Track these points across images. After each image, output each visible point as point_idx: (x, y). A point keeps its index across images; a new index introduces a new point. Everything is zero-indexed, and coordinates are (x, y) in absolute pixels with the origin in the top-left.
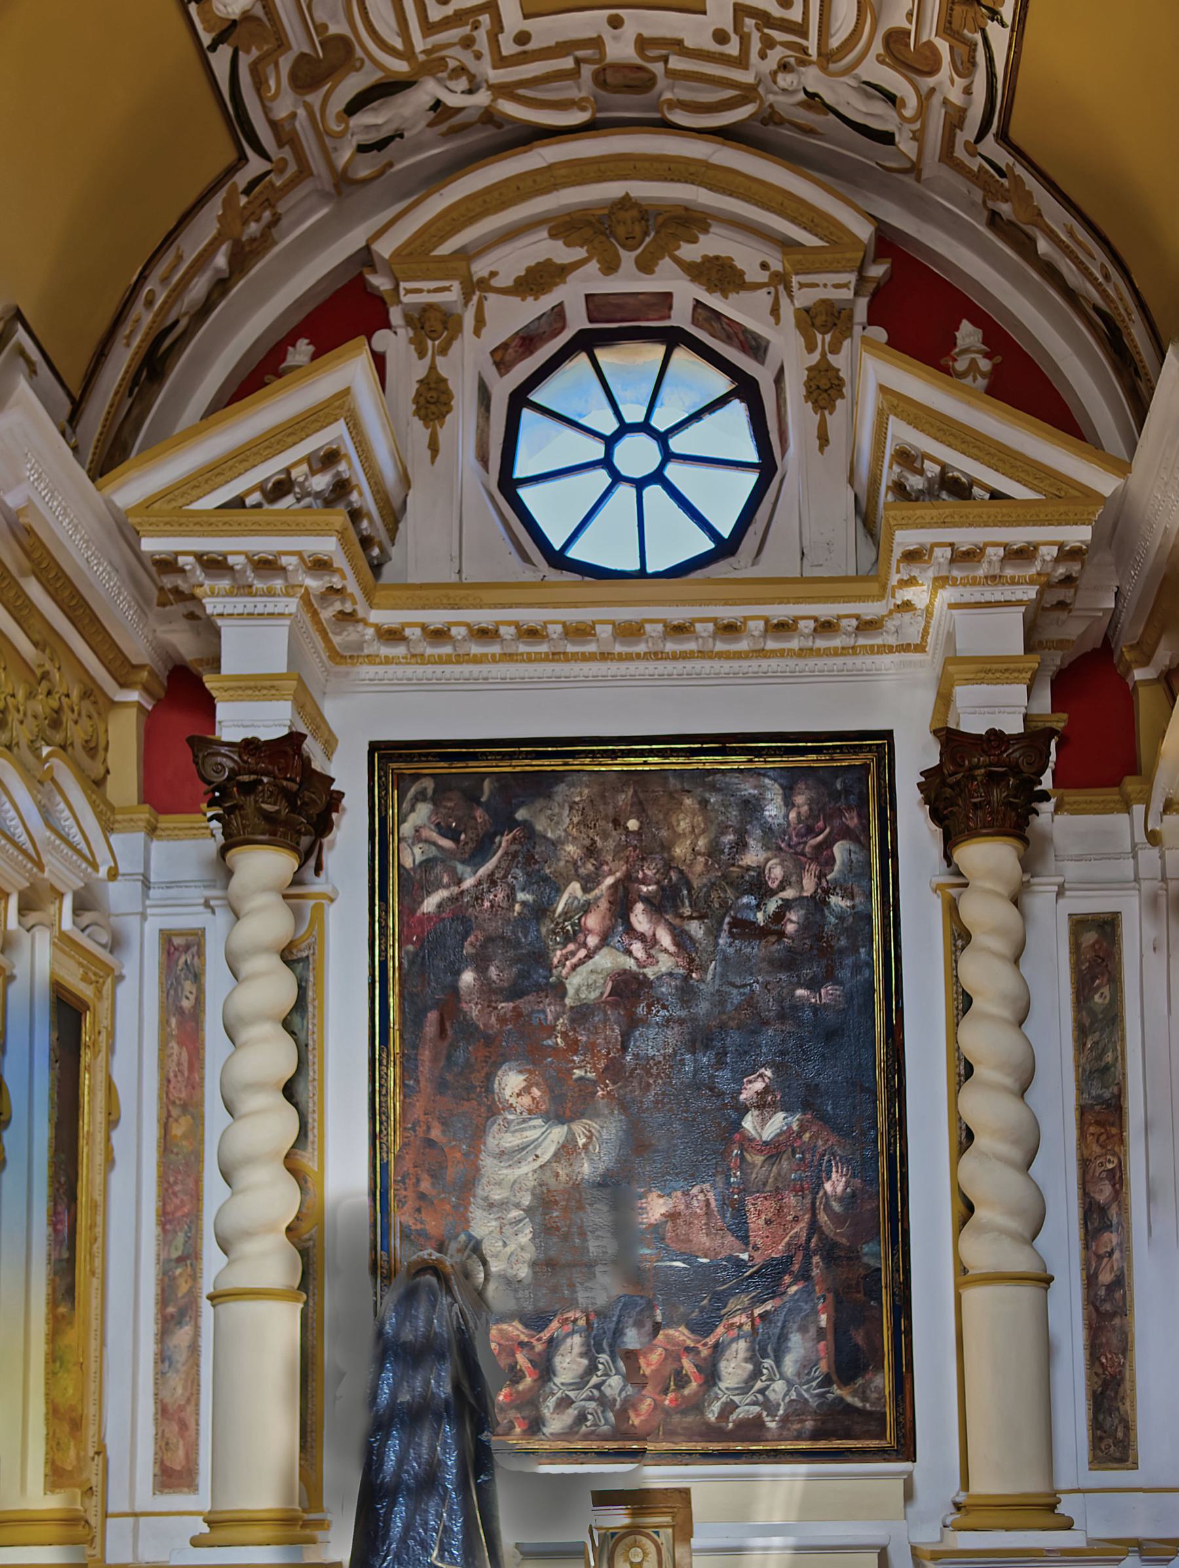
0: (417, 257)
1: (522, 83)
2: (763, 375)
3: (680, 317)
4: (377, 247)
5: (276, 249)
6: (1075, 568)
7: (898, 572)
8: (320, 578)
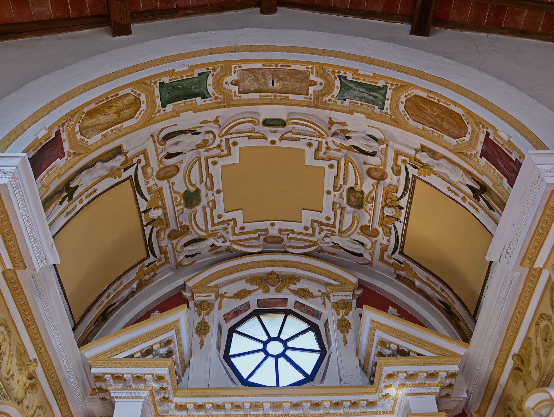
0: (202, 286)
1: (240, 240)
2: (320, 324)
3: (290, 306)
4: (187, 284)
5: (153, 284)
6: (453, 381)
7: (384, 382)
8: (159, 383)
